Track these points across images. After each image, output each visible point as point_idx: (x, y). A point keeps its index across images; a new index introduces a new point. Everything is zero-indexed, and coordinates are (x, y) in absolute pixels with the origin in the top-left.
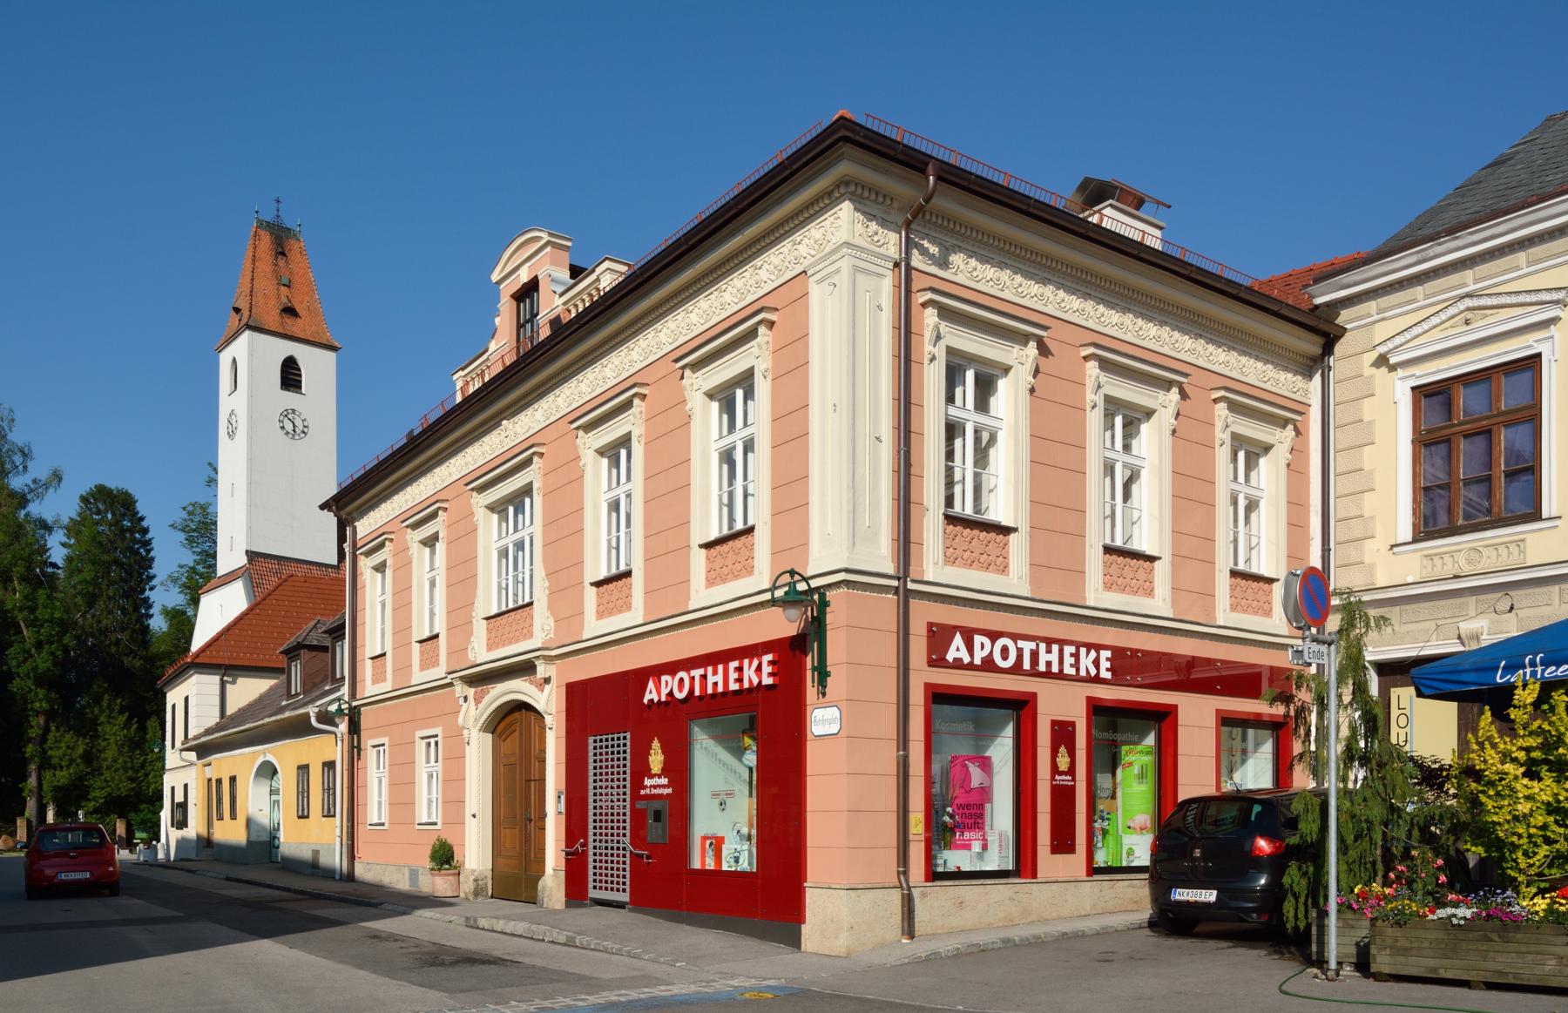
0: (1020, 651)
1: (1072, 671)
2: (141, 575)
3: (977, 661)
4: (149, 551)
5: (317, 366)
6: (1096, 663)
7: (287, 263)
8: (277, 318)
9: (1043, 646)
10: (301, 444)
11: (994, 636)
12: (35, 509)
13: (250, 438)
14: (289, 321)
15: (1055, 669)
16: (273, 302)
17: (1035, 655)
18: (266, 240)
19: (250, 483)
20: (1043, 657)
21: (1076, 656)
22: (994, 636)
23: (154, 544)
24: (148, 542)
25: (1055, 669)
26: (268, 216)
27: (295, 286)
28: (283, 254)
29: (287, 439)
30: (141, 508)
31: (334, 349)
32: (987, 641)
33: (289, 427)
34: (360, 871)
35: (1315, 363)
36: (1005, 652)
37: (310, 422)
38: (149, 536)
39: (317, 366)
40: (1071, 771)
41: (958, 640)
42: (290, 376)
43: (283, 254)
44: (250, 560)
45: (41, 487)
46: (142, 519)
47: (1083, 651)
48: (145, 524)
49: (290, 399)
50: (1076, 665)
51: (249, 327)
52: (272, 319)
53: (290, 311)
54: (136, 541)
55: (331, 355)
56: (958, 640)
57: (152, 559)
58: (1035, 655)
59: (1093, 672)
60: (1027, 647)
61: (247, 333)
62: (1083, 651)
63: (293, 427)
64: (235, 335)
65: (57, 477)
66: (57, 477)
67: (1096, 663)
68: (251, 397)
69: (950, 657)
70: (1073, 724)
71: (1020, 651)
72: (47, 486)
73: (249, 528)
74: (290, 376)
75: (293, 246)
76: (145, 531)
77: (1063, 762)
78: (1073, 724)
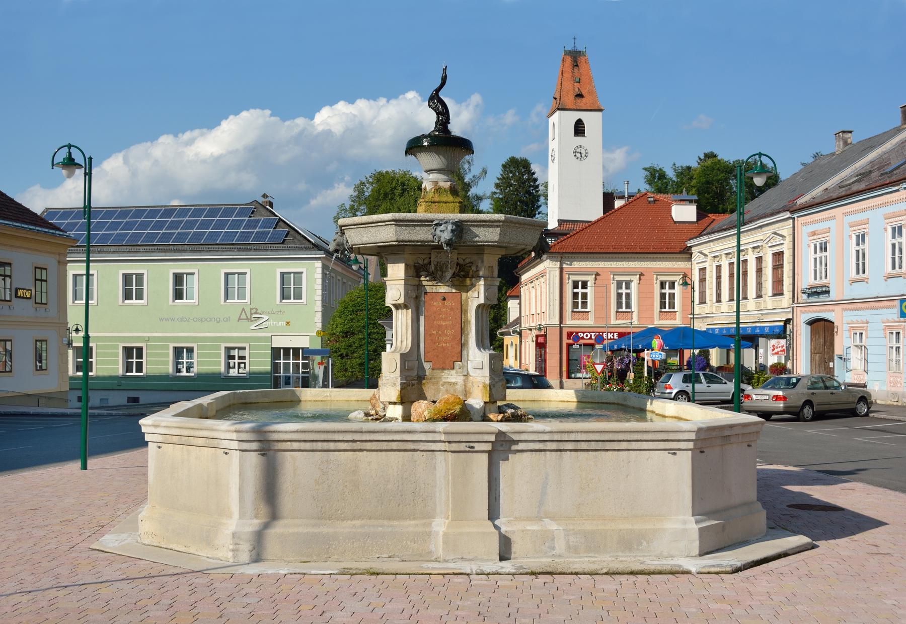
2: (533, 206)
8: (573, 100)
10: (585, 162)
11: (584, 333)
12: (473, 191)
13: (560, 163)
14: (579, 100)
16: (571, 92)
18: (569, 60)
19: (559, 186)
22: (584, 333)
26: (569, 48)
27: (582, 81)
28: (577, 66)
29: (578, 161)
31: (601, 110)
33: (578, 155)
35: (690, 259)
37: (589, 151)
38: (537, 183)
42: (579, 129)
43: (577, 66)
44: (559, 225)
45: (476, 179)
46: (534, 173)
48: (535, 176)
49: (579, 140)
51: (559, 109)
52: (570, 100)
53: (580, 96)
54: (531, 186)
55: (600, 114)
61: (558, 112)
63: (580, 154)
64: (554, 112)
65: (484, 172)
66: (484, 172)
68: (560, 143)
72: (479, 178)
73: (559, 208)
74: (579, 129)
75: (582, 60)
76: (536, 180)
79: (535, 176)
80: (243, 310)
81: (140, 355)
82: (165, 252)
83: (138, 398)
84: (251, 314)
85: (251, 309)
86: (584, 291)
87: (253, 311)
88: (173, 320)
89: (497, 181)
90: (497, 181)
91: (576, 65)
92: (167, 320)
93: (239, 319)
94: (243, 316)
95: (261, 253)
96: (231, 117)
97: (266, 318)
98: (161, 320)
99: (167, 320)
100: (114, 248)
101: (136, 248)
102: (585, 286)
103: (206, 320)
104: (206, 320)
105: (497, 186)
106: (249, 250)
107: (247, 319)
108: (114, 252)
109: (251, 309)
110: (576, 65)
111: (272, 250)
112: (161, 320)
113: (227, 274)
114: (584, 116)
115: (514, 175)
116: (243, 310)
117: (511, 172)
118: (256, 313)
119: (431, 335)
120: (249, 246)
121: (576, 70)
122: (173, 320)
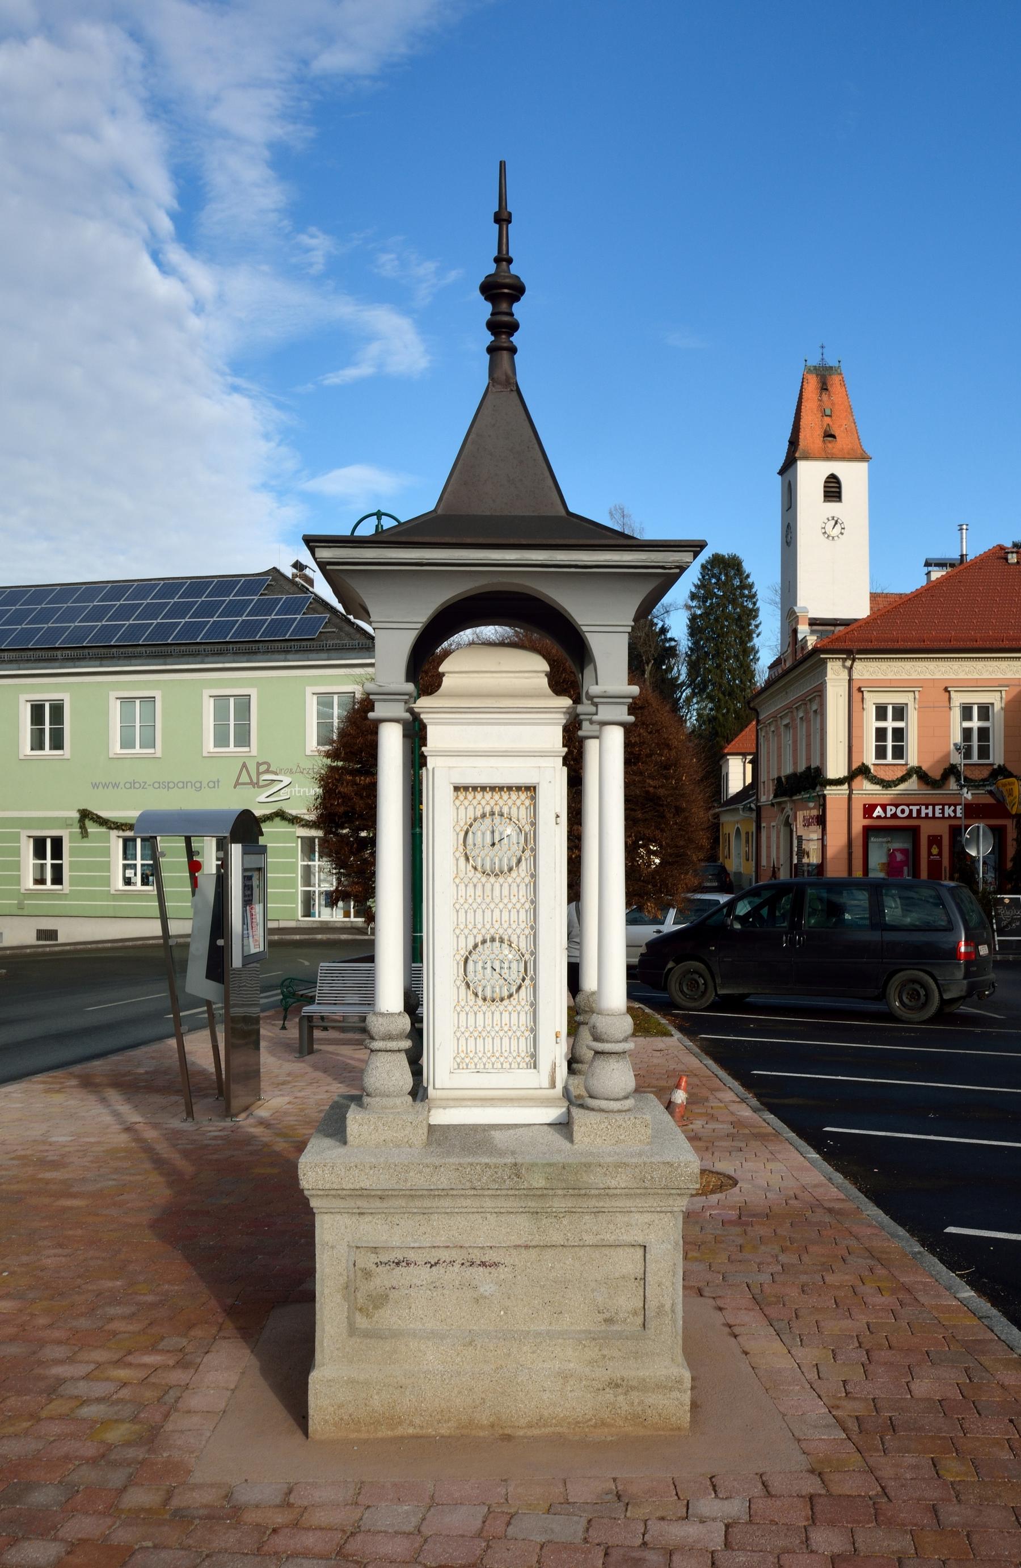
0: (911, 811)
1: (952, 815)
3: (889, 815)
4: (755, 604)
5: (854, 476)
6: (955, 811)
7: (829, 395)
9: (923, 807)
15: (930, 815)
17: (919, 811)
20: (924, 812)
21: (943, 810)
23: (758, 597)
24: (754, 596)
25: (930, 815)
26: (814, 361)
28: (827, 389)
30: (747, 567)
32: (894, 809)
34: (402, 521)
36: (903, 811)
38: (754, 590)
39: (854, 476)
40: (940, 854)
41: (879, 809)
43: (827, 389)
46: (748, 576)
47: (946, 807)
49: (833, 507)
50: (943, 813)
53: (829, 435)
56: (879, 809)
57: (758, 609)
58: (919, 811)
59: (952, 815)
60: (915, 808)
62: (946, 807)
67: (955, 811)
69: (875, 815)
70: (941, 836)
71: (911, 811)
75: (834, 380)
76: (751, 586)
77: (935, 850)
78: (941, 836)
79: (750, 580)
80: (244, 765)
81: (57, 853)
82: (101, 658)
83: (56, 932)
84: (259, 774)
85: (259, 764)
86: (881, 724)
87: (263, 768)
88: (116, 785)
89: (693, 589)
90: (693, 589)
91: (824, 387)
92: (106, 786)
93: (237, 784)
94: (245, 778)
95: (276, 656)
96: (565, 769)
97: (286, 780)
98: (95, 786)
99: (106, 786)
100: (12, 654)
101: (50, 653)
102: (900, 713)
103: (176, 785)
104: (176, 785)
105: (697, 586)
106: (255, 653)
107: (252, 783)
108: (11, 661)
109: (259, 764)
110: (824, 387)
111: (297, 651)
112: (95, 786)
113: (531, 789)
114: (840, 468)
115: (719, 579)
116: (244, 765)
117: (714, 576)
118: (267, 771)
119: (328, 841)
120: (254, 646)
121: (825, 397)
122: (116, 785)
